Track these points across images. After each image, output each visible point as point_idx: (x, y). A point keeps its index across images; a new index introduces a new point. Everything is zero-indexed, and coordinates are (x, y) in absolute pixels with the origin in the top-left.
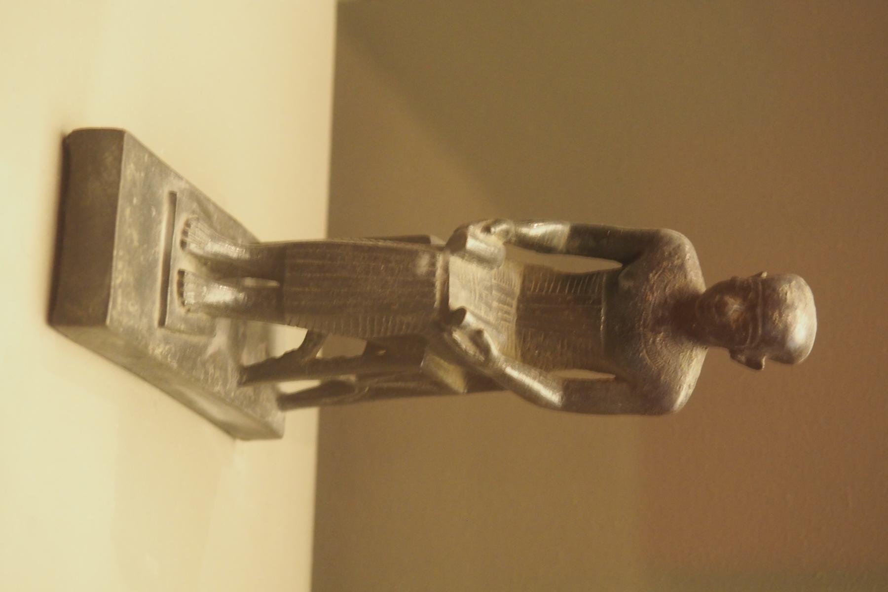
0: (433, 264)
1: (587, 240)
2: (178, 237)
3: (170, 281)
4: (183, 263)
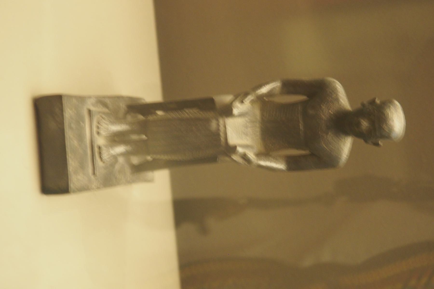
0: (218, 125)
1: (290, 86)
2: (95, 129)
3: (95, 151)
4: (100, 141)
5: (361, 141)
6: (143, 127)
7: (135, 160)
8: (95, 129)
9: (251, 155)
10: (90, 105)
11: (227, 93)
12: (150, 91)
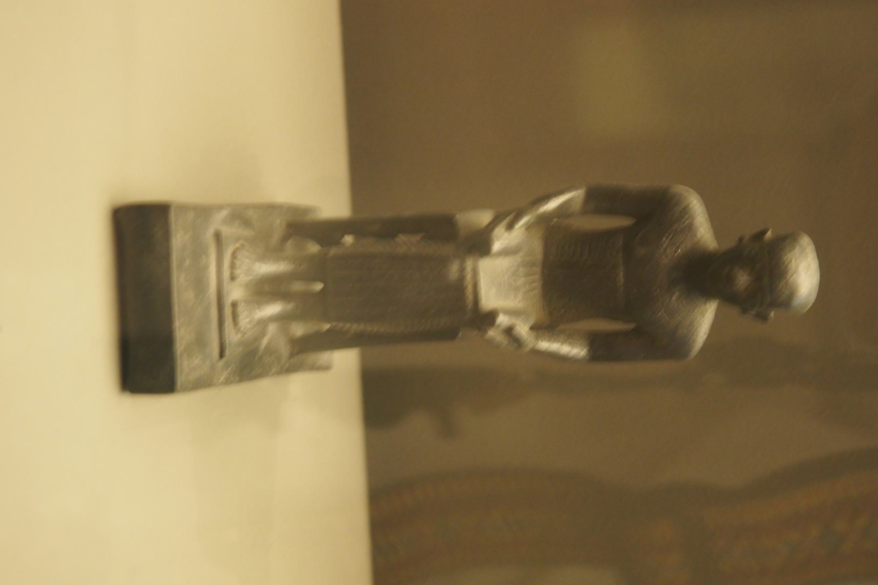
0: (462, 270)
1: (601, 199)
2: (226, 274)
4: (236, 293)
5: (733, 312)
6: (317, 269)
7: (299, 330)
8: (226, 274)
9: (523, 329)
10: (217, 222)
11: (480, 205)
12: (333, 203)
